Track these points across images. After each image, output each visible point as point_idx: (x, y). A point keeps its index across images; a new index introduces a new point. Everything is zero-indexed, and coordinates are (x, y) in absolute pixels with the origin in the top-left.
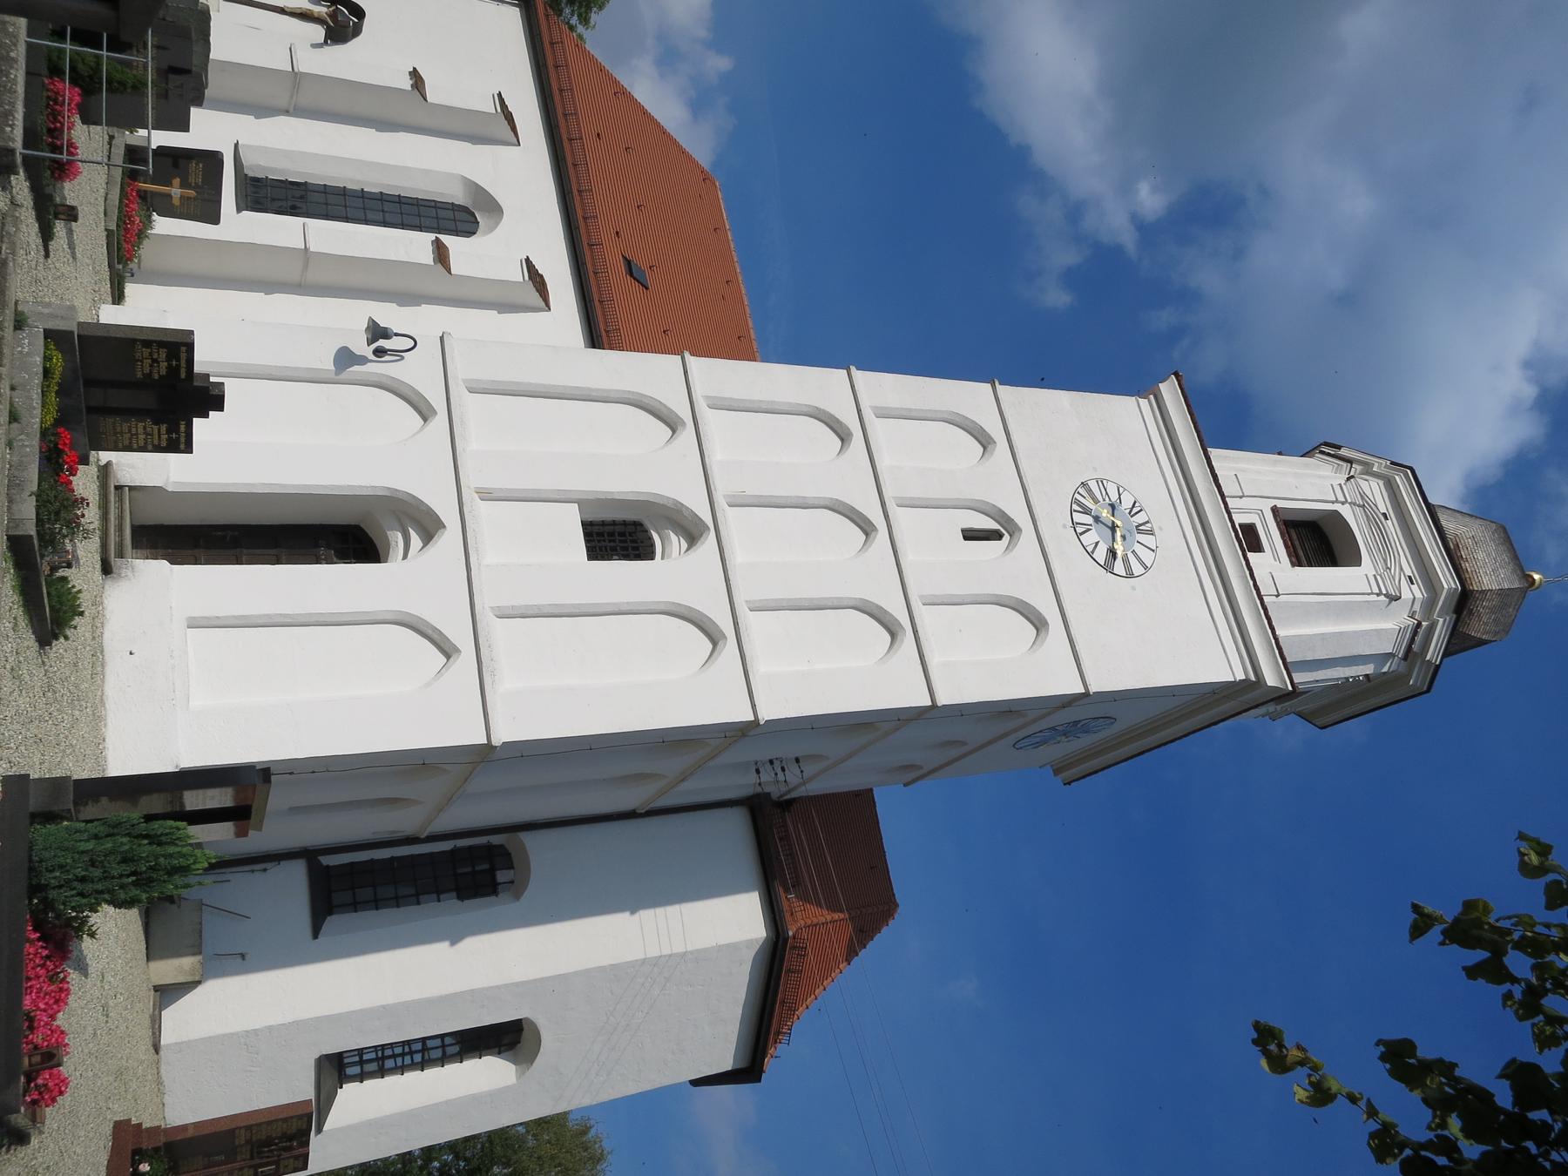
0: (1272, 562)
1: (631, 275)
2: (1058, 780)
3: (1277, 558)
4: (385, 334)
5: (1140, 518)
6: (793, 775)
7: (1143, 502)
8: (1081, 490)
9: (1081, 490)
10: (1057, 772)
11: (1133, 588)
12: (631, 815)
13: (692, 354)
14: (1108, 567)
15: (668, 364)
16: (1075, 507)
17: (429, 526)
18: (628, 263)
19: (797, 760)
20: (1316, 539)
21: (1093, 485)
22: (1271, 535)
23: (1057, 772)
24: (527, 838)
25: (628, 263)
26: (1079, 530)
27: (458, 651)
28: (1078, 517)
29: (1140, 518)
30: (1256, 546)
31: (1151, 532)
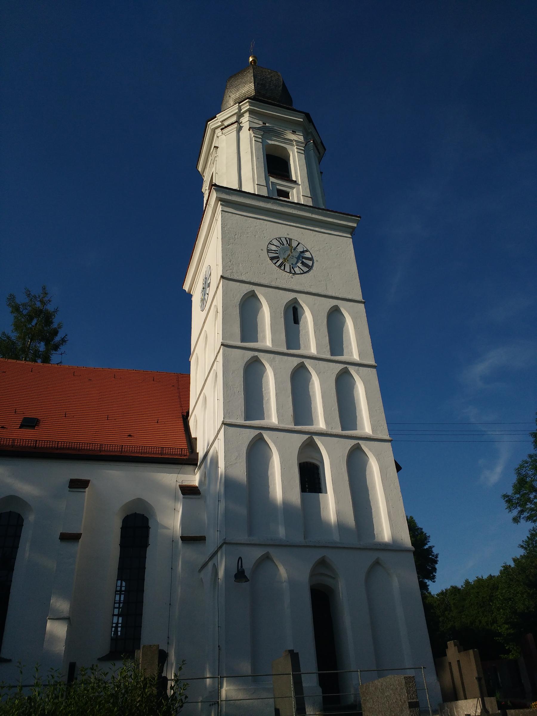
8: (275, 262)
17: (323, 563)
30: (286, 194)
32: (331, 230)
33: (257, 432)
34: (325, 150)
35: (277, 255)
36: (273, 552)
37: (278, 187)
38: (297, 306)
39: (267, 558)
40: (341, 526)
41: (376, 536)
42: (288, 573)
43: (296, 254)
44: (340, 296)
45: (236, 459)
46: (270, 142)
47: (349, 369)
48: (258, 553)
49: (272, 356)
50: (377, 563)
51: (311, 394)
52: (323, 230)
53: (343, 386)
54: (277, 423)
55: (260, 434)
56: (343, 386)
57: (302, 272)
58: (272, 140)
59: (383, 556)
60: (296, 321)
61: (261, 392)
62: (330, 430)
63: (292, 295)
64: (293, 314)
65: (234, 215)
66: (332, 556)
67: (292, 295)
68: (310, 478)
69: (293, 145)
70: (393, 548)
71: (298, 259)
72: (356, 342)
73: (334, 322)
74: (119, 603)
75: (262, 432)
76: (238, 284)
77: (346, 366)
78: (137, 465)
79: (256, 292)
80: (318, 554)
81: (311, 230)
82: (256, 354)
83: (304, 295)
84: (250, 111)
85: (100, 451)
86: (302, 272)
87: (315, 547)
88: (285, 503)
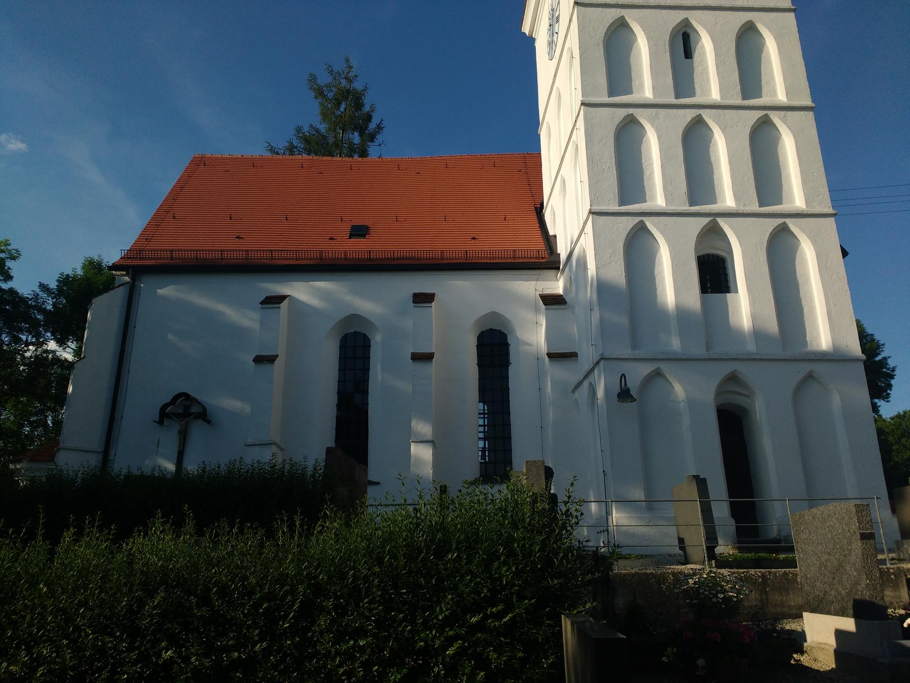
6: (252, 255)
17: (733, 378)
27: (811, 371)
36: (664, 367)
38: (689, 31)
40: (758, 334)
42: (688, 393)
47: (771, 116)
48: (645, 369)
49: (654, 111)
51: (712, 159)
60: (688, 53)
61: (641, 164)
64: (684, 43)
68: (714, 274)
77: (765, 112)
79: (627, 18)
80: (726, 369)
82: (631, 111)
83: (700, 12)
85: (346, 259)
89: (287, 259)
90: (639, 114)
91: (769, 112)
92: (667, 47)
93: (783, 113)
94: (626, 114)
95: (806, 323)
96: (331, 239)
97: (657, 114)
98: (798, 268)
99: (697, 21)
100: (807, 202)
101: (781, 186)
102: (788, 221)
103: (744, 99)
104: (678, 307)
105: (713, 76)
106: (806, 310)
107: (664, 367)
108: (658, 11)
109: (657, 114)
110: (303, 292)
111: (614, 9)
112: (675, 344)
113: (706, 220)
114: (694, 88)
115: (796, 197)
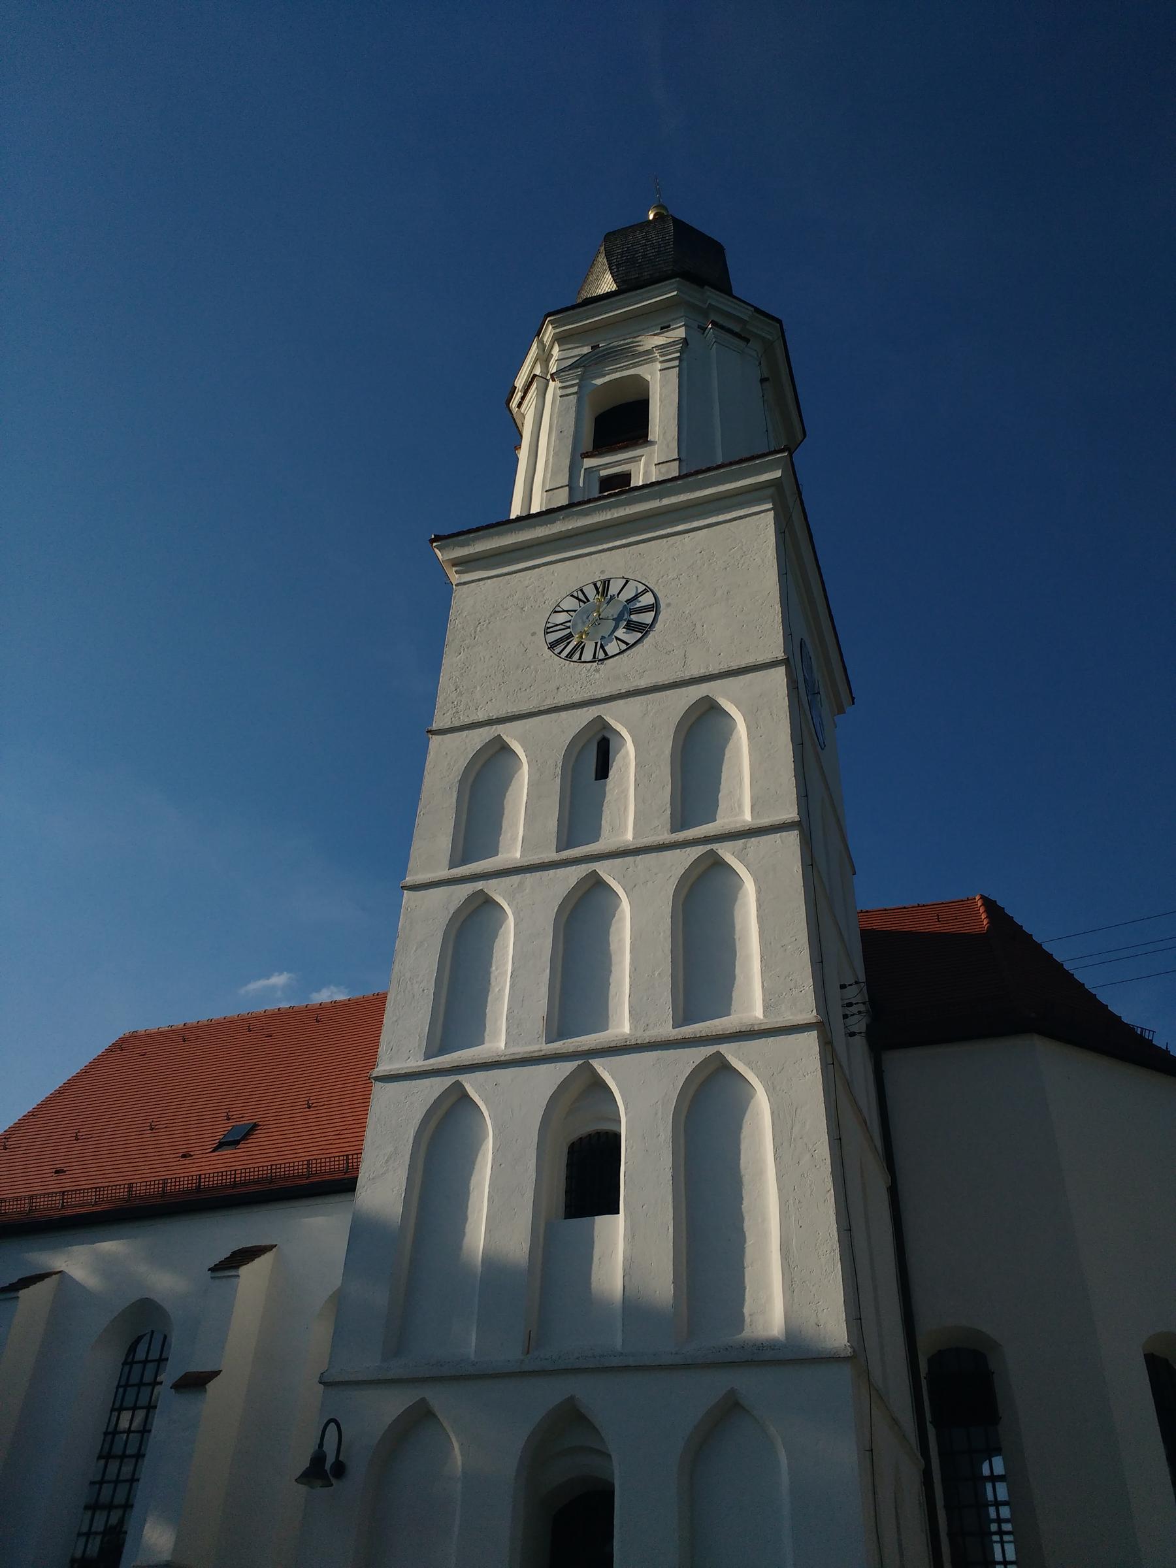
0: (646, 465)
1: (237, 1142)
2: (849, 709)
3: (636, 459)
4: (318, 1459)
5: (591, 592)
6: (37, 1203)
7: (573, 586)
8: (557, 650)
9: (557, 650)
10: (841, 711)
11: (669, 605)
12: (894, 1193)
13: (374, 1065)
14: (644, 630)
15: (383, 1097)
16: (576, 657)
17: (571, 1418)
18: (221, 1145)
19: (843, 987)
20: (618, 422)
21: (552, 637)
22: (608, 464)
23: (841, 711)
24: (927, 1325)
25: (221, 1145)
26: (601, 655)
27: (732, 1392)
28: (588, 655)
29: (591, 592)
30: (626, 477)
31: (606, 583)
32: (718, 515)
33: (448, 1081)
34: (779, 321)
35: (568, 631)
36: (438, 1399)
37: (603, 473)
38: (607, 735)
39: (420, 1417)
40: (634, 1309)
41: (747, 1319)
42: (477, 1455)
43: (612, 611)
44: (713, 669)
45: (387, 1161)
46: (599, 382)
47: (720, 852)
48: (390, 1406)
49: (515, 879)
50: (731, 1408)
51: (613, 947)
52: (695, 524)
53: (701, 906)
54: (761, 1017)
55: (458, 1085)
56: (701, 906)
57: (624, 647)
58: (604, 376)
59: (746, 1383)
60: (603, 771)
61: (488, 973)
62: (639, 1033)
63: (586, 716)
64: (597, 754)
65: (482, 583)
66: (596, 1397)
67: (586, 716)
68: (587, 1176)
69: (653, 360)
70: (792, 1356)
71: (617, 621)
72: (755, 773)
73: (698, 744)
74: (1001, 1533)
75: (460, 1078)
76: (465, 733)
77: (709, 847)
78: (319, 1200)
79: (504, 737)
80: (547, 1396)
81: (538, 566)
82: (479, 885)
83: (621, 702)
84: (560, 339)
85: (163, 1194)
86: (624, 647)
87: (626, 1368)
88: (489, 1262)
89: (81, 1206)
90: (604, 869)
91: (714, 846)
92: (559, 770)
93: (740, 843)
94: (471, 892)
95: (748, 1272)
96: (184, 1156)
97: (521, 884)
98: (744, 1146)
99: (617, 717)
100: (766, 1008)
101: (732, 978)
102: (725, 1049)
103: (673, 830)
104: (487, 1261)
105: (632, 803)
106: (750, 1241)
107: (438, 1399)
108: (554, 716)
109: (521, 884)
110: (78, 1262)
111: (487, 728)
112: (468, 1342)
113: (569, 1067)
114: (599, 828)
115: (752, 1002)
